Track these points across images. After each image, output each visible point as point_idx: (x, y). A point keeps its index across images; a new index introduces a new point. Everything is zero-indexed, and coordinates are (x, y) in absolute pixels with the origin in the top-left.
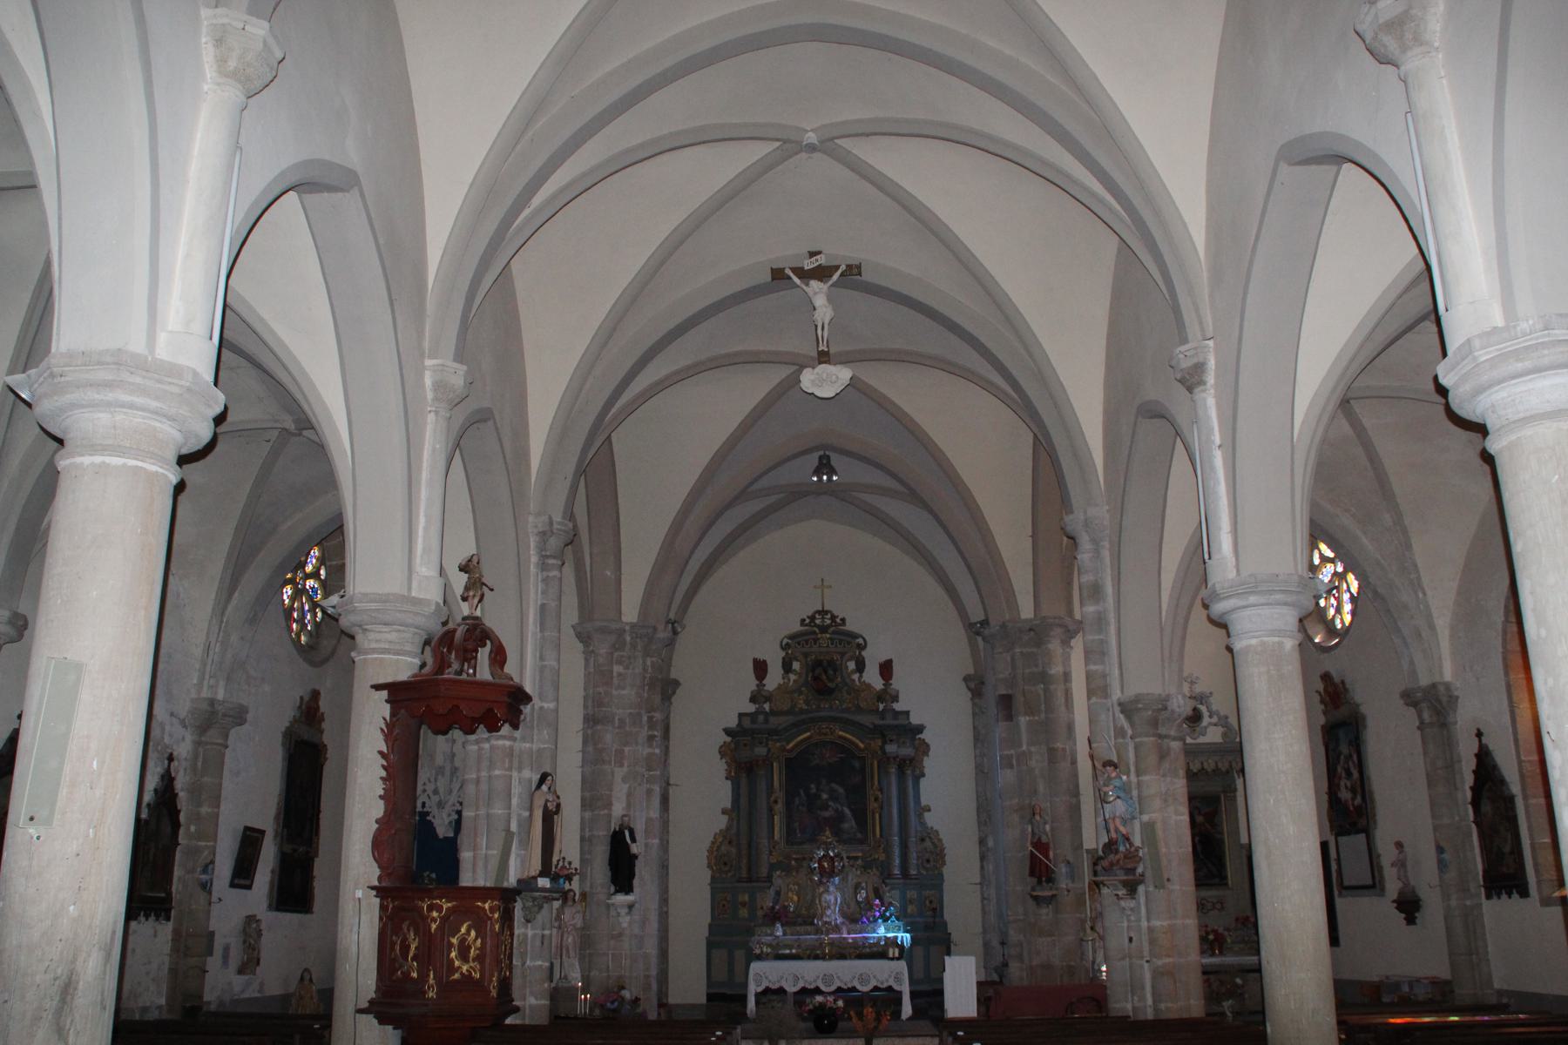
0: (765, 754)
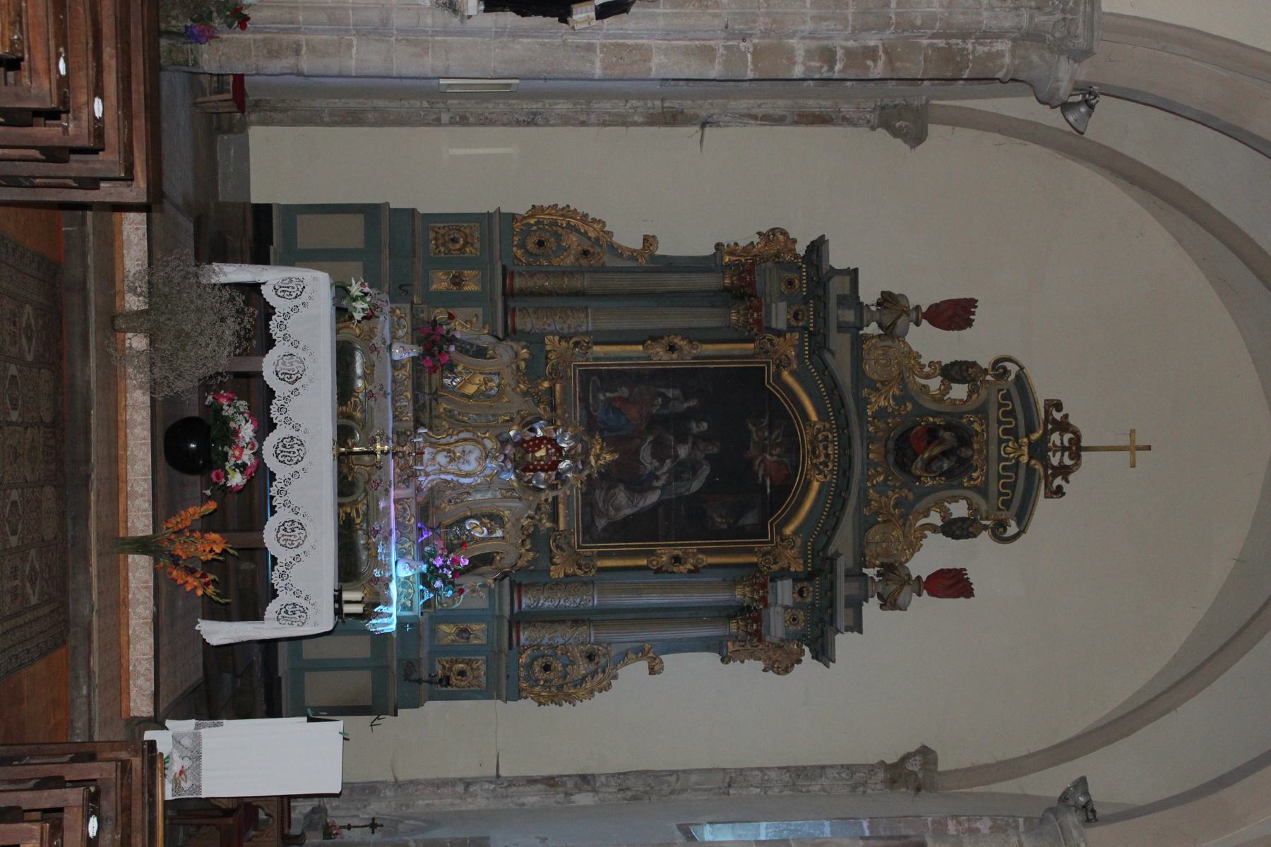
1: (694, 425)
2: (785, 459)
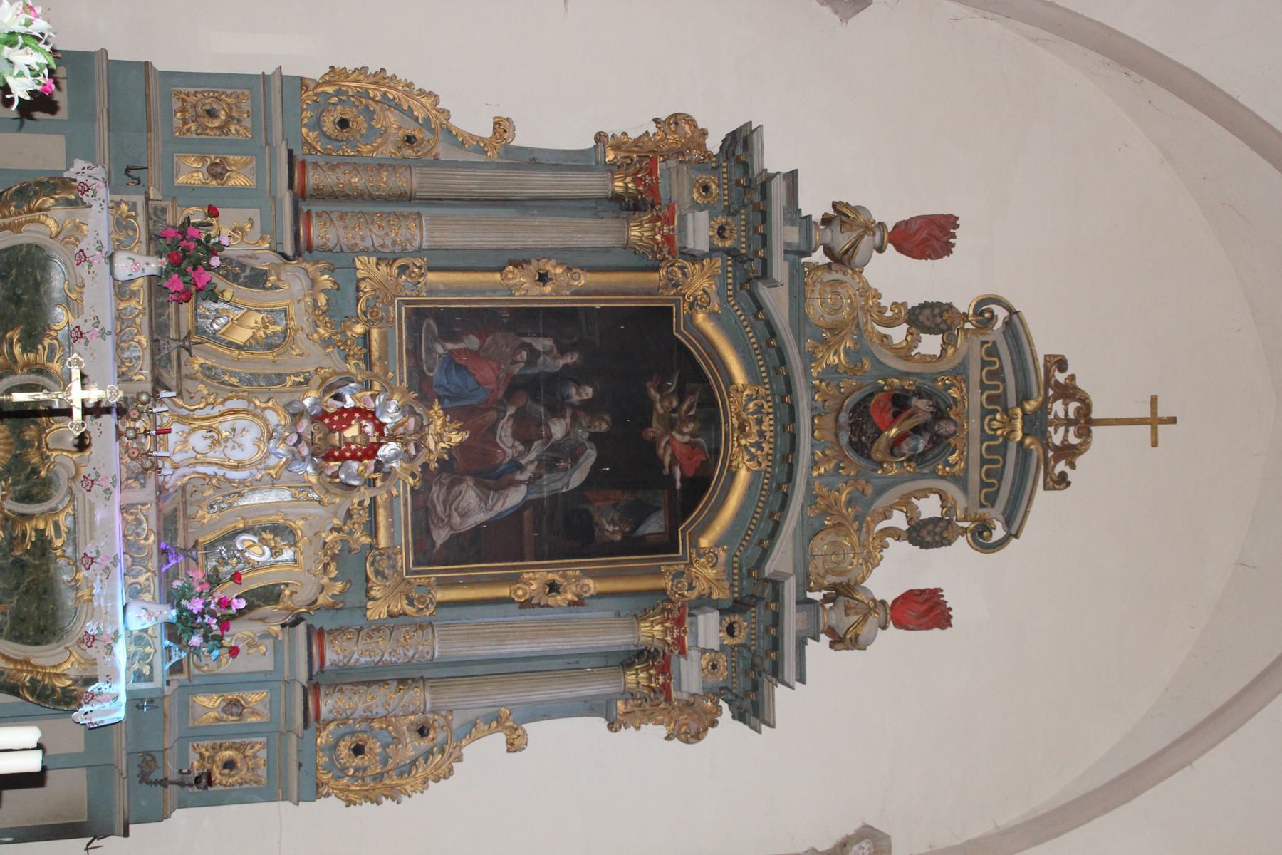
0: (690, 245)
1: (574, 390)
2: (701, 440)
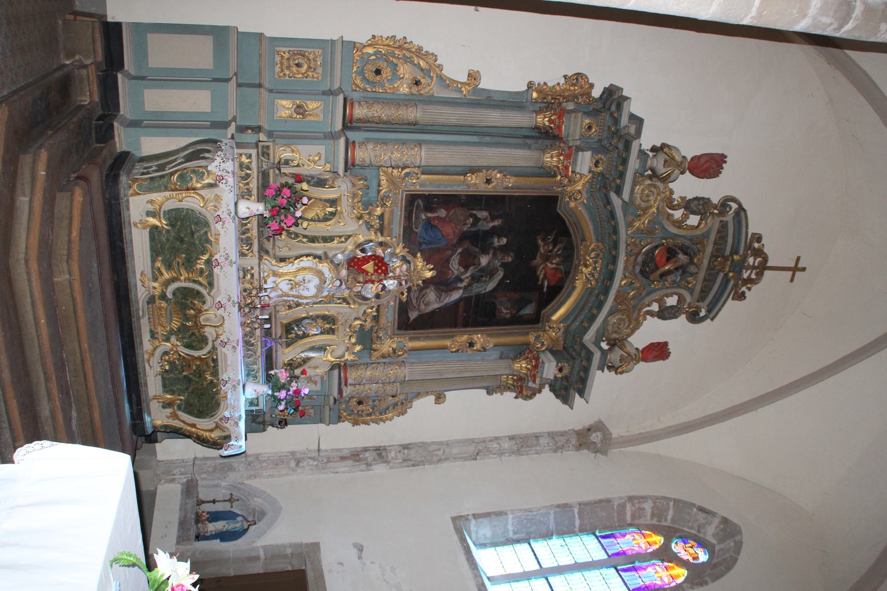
1: (496, 240)
2: (561, 267)
